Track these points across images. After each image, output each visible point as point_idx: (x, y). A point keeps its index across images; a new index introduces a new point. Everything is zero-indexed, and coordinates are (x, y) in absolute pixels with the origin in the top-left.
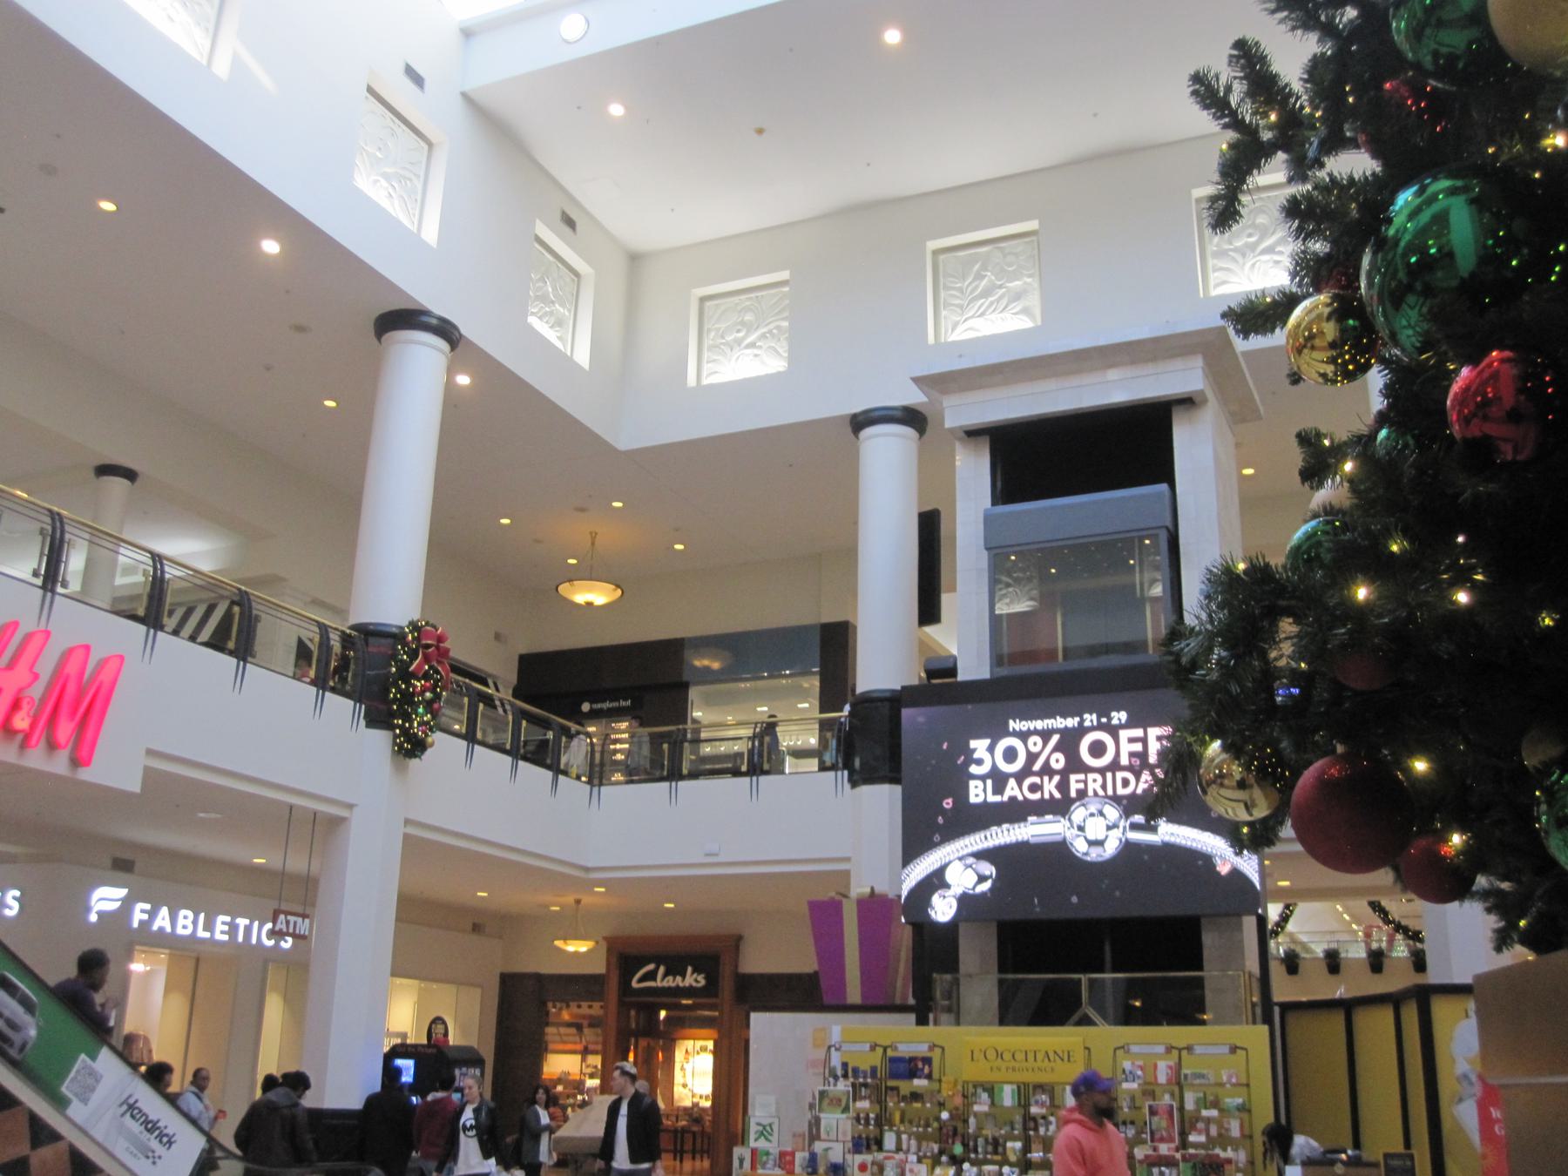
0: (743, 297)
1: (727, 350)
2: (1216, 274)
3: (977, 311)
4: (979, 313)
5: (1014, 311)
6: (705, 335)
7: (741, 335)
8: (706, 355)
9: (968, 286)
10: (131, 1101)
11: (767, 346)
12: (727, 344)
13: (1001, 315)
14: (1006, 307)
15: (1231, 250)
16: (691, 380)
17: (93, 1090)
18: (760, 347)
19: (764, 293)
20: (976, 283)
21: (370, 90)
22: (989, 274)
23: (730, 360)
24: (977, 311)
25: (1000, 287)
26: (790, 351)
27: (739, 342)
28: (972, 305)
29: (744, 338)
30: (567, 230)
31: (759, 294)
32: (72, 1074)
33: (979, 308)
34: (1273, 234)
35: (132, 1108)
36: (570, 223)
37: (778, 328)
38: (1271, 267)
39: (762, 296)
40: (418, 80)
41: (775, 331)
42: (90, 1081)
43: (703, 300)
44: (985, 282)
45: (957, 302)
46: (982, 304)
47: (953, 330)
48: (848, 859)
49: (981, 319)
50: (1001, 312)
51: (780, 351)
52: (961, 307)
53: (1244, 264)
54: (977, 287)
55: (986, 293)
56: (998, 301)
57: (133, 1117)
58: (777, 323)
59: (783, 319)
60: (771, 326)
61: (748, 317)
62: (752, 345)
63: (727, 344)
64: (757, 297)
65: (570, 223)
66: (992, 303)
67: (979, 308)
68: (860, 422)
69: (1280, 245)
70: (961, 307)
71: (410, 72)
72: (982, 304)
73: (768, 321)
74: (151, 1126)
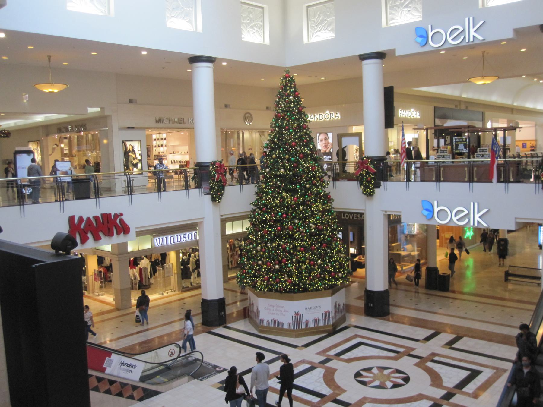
2: (390, 16)
8: (389, 11)
10: (122, 362)
12: (396, 6)
16: (305, 41)
17: (111, 364)
18: (410, 7)
20: (319, 18)
23: (398, 13)
25: (325, 20)
26: (423, 9)
27: (402, 5)
29: (403, 3)
32: (105, 362)
35: (123, 364)
38: (407, 13)
42: (110, 362)
43: (308, 7)
44: (321, 18)
46: (320, 27)
47: (312, 36)
48: (400, 212)
49: (320, 32)
51: (419, 9)
53: (399, 11)
54: (318, 20)
56: (325, 25)
57: (123, 365)
62: (407, 6)
63: (396, 6)
66: (323, 27)
68: (364, 57)
72: (320, 27)
74: (129, 365)
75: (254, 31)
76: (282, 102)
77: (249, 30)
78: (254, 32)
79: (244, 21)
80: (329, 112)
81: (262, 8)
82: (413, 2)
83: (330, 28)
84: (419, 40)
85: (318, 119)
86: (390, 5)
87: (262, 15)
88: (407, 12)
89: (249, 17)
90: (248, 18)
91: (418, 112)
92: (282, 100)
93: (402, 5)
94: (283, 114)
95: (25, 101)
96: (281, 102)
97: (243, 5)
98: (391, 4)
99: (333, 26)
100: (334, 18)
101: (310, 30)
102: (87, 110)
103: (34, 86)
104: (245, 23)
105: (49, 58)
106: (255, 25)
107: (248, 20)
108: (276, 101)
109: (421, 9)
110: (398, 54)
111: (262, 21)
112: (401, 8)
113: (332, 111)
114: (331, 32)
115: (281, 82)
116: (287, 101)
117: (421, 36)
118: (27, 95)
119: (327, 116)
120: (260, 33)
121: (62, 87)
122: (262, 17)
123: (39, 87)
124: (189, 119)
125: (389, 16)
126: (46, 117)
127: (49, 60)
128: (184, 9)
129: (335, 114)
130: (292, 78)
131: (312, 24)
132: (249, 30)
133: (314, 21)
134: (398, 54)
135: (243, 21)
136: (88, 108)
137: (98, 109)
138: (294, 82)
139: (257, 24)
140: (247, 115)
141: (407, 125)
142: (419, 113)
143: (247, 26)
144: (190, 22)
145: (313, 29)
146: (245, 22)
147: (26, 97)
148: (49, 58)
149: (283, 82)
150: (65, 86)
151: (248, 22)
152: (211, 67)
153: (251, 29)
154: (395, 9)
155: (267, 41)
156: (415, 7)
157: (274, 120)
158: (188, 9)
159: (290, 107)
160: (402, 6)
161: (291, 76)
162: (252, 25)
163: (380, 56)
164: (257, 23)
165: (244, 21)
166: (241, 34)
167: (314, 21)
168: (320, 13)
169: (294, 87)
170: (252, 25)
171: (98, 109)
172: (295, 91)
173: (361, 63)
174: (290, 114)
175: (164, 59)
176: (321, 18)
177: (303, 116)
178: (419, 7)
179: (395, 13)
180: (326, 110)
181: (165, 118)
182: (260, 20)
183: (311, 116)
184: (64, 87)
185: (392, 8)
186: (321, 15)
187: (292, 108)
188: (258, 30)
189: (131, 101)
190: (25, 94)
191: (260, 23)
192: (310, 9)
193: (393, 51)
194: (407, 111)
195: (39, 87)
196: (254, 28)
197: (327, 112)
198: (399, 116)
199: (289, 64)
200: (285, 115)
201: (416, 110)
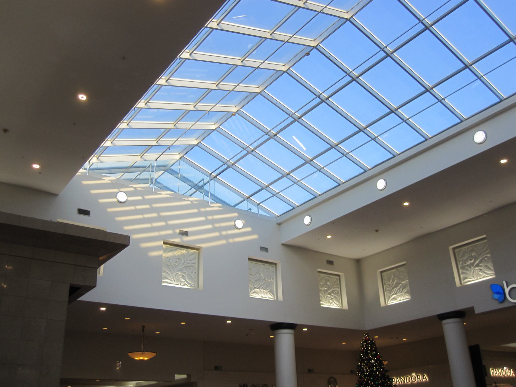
0: (469, 246)
1: (469, 268)
2: (463, 275)
3: (395, 292)
4: (395, 293)
5: (405, 292)
6: (458, 263)
7: (472, 261)
8: (460, 271)
9: (391, 283)
11: (484, 265)
12: (468, 266)
13: (401, 294)
14: (402, 290)
15: (466, 266)
16: (382, 303)
18: (481, 266)
19: (477, 243)
20: (393, 282)
21: (250, 259)
22: (396, 279)
23: (471, 272)
24: (395, 292)
25: (400, 283)
26: (494, 266)
27: (472, 264)
28: (393, 290)
30: (330, 266)
31: (475, 244)
33: (395, 291)
34: (478, 258)
36: (330, 263)
37: (486, 257)
38: (479, 272)
39: (477, 245)
40: (266, 249)
41: (486, 259)
43: (382, 272)
44: (395, 282)
45: (389, 289)
46: (395, 290)
50: (401, 292)
51: (490, 267)
52: (389, 290)
53: (471, 271)
54: (394, 283)
55: (396, 286)
56: (400, 288)
58: (486, 255)
59: (487, 254)
60: (484, 256)
61: (473, 254)
62: (478, 265)
64: (475, 245)
65: (330, 263)
66: (398, 289)
67: (395, 291)
69: (480, 263)
70: (389, 290)
71: (262, 248)
72: (395, 290)
73: (482, 255)
75: (332, 297)
76: (364, 366)
77: (327, 297)
78: (332, 298)
79: (322, 288)
80: (416, 374)
81: (339, 275)
82: (483, 261)
83: (405, 290)
84: (497, 296)
85: (405, 382)
86: (461, 266)
87: (339, 282)
88: (479, 271)
89: (326, 284)
90: (326, 286)
91: (511, 370)
92: (364, 364)
93: (472, 264)
94: (366, 379)
95: (118, 368)
96: (363, 366)
97: (320, 274)
98: (462, 264)
99: (408, 288)
100: (408, 281)
101: (386, 293)
102: (174, 376)
103: (127, 354)
104: (323, 291)
105: (143, 327)
106: (333, 292)
107: (326, 287)
108: (358, 365)
109: (492, 267)
110: (477, 311)
111: (339, 288)
112: (472, 268)
113: (419, 373)
114: (407, 294)
115: (361, 345)
116: (369, 365)
117: (498, 293)
118: (121, 363)
119: (414, 379)
120: (338, 299)
121: (152, 355)
122: (339, 283)
123: (131, 355)
124: (273, 385)
125: (462, 276)
126: (137, 383)
127: (143, 330)
128: (266, 280)
129: (422, 376)
130: (372, 342)
131: (388, 287)
132: (327, 297)
133: (389, 285)
134: (477, 311)
135: (321, 289)
136: (175, 375)
137: (184, 376)
138: (375, 345)
139: (334, 291)
140: (332, 380)
141: (502, 384)
142: (513, 371)
143: (325, 293)
144: (271, 292)
145: (388, 292)
146: (323, 289)
147: (120, 364)
148: (143, 327)
149: (363, 345)
150: (155, 354)
151: (326, 289)
152: (292, 333)
153: (329, 296)
154: (467, 269)
155: (346, 306)
156: (486, 266)
157: (357, 385)
158: (269, 280)
159: (373, 371)
160: (473, 265)
161: (371, 340)
162: (329, 291)
163: (459, 314)
164: (335, 289)
165: (322, 288)
166: (320, 301)
167: (389, 285)
168: (394, 277)
169: (376, 350)
170: (329, 291)
171: (184, 376)
172: (376, 354)
173: (441, 323)
174: (374, 379)
175: (248, 327)
176: (395, 282)
177: (387, 380)
178: (490, 265)
179: (467, 272)
180: (413, 373)
181: (250, 384)
182: (337, 287)
183: (397, 379)
184: (153, 355)
185: (463, 268)
186: (395, 279)
187: (374, 372)
188: (336, 296)
189: (216, 368)
190: (119, 361)
191: (338, 289)
192: (383, 274)
193: (472, 309)
194: (500, 370)
195: (131, 355)
196: (333, 294)
197: (414, 374)
198: (492, 375)
199: (369, 326)
200: (369, 380)
201: (510, 368)
